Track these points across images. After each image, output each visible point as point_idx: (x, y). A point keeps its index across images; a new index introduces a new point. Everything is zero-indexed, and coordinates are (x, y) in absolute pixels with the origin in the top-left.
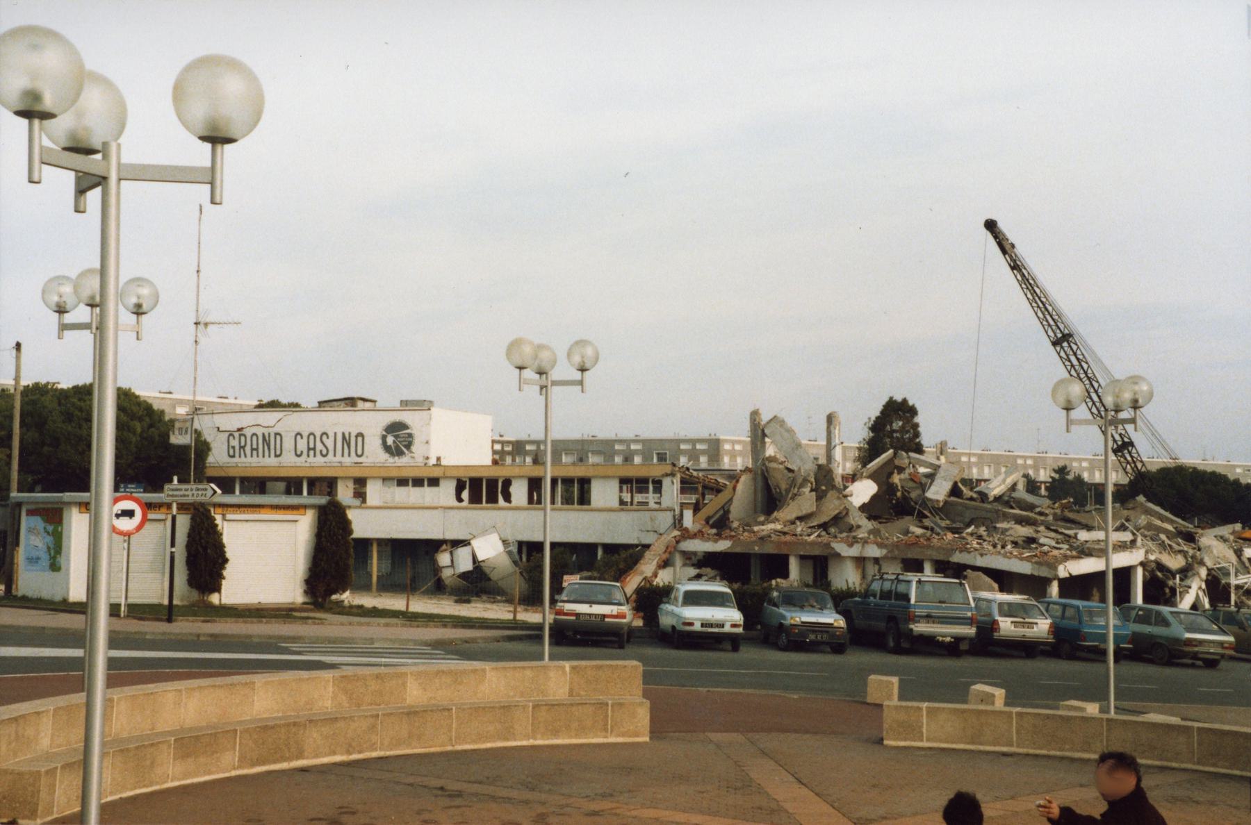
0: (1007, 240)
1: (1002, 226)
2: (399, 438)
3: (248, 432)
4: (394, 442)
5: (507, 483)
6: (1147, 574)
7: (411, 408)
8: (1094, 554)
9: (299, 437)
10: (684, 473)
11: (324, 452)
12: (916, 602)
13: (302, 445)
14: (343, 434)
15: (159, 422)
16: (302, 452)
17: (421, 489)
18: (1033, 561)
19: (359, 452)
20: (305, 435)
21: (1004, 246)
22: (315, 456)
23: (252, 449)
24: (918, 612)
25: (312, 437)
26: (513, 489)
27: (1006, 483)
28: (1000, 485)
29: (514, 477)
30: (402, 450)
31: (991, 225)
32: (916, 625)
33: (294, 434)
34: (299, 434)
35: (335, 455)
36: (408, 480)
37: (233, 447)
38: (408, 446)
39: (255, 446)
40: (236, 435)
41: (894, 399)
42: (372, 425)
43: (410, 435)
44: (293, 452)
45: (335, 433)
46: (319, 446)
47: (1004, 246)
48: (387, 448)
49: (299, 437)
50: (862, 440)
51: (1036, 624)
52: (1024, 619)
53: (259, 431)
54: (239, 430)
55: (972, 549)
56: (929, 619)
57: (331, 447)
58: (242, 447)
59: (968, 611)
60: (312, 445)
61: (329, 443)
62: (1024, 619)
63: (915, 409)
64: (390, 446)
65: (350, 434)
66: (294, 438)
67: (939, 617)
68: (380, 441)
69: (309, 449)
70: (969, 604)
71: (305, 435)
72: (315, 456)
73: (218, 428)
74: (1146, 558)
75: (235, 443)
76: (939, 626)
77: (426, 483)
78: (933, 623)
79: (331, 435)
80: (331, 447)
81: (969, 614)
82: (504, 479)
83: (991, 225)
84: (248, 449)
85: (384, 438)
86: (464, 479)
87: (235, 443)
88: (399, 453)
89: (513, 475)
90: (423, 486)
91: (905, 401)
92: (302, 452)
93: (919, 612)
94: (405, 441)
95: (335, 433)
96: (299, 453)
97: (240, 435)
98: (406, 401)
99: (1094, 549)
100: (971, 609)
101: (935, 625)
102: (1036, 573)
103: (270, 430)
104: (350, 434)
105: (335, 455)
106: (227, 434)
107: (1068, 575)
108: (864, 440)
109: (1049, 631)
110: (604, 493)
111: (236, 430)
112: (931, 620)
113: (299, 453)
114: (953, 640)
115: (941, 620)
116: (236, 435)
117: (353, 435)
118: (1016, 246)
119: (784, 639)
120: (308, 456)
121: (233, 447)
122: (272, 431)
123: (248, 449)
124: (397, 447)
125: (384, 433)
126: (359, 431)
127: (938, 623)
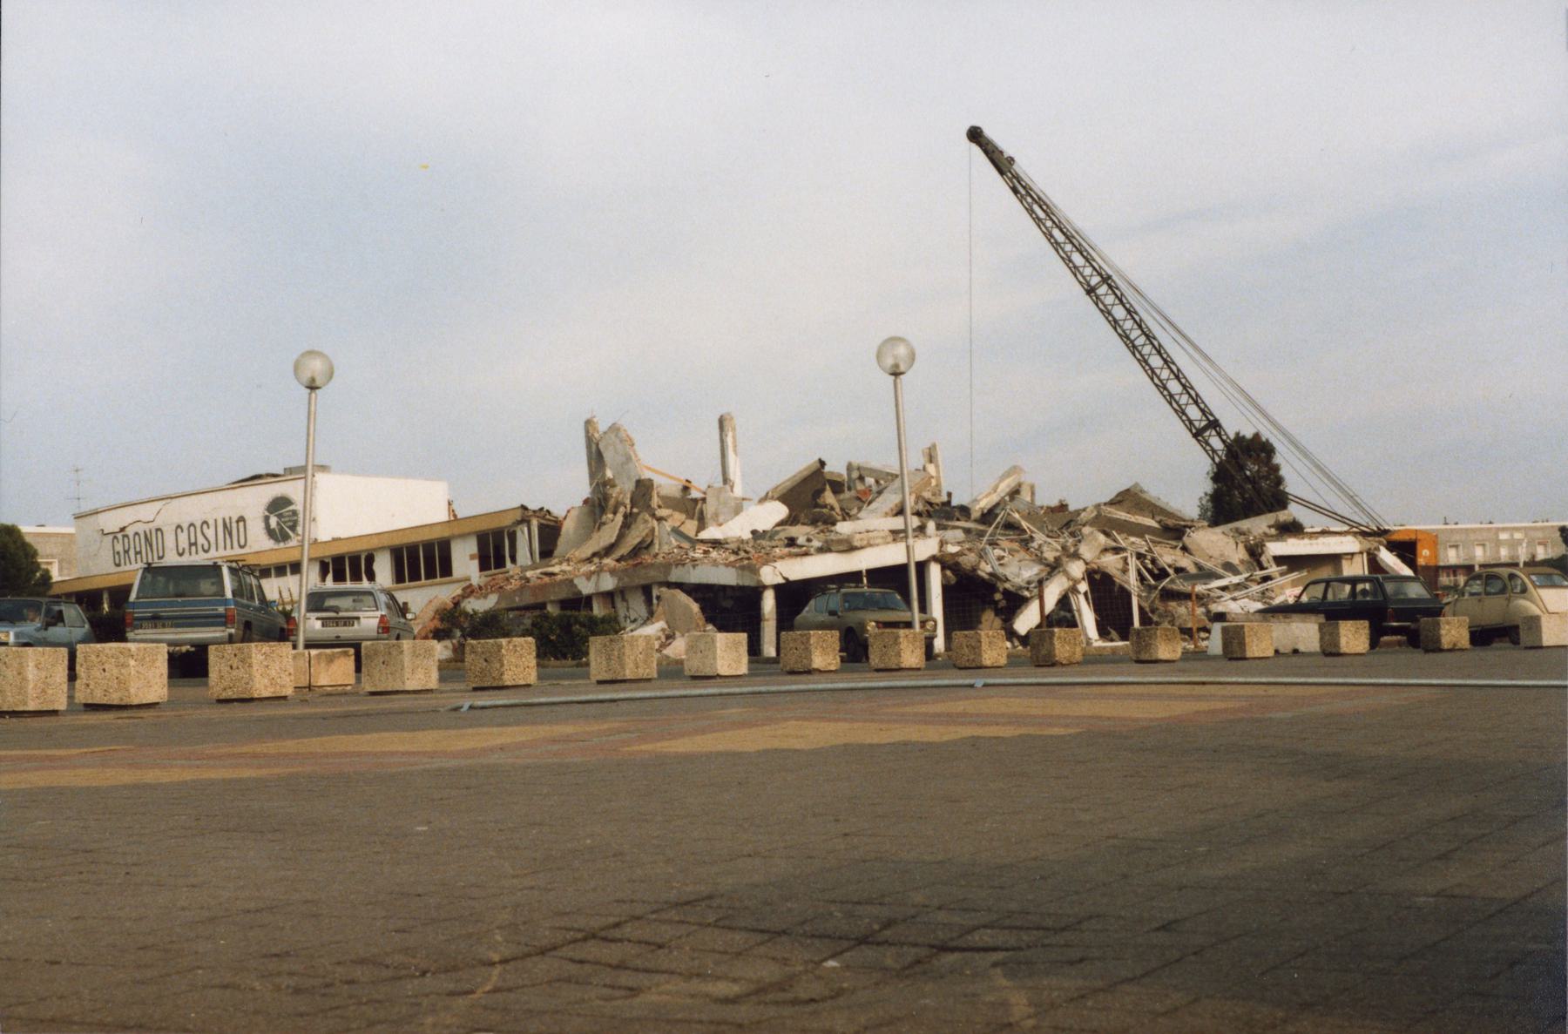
0: (1001, 152)
1: (990, 132)
2: (283, 517)
3: (130, 531)
4: (278, 524)
5: (370, 559)
6: (948, 573)
7: (297, 476)
8: (833, 548)
9: (179, 530)
10: (543, 518)
11: (206, 547)
12: (138, 598)
13: (183, 538)
14: (224, 520)
15: (528, 582)
16: (184, 549)
17: (269, 579)
18: (737, 565)
19: (242, 543)
20: (185, 526)
21: (1000, 162)
22: (197, 553)
23: (137, 553)
24: (136, 613)
25: (192, 528)
26: (376, 567)
27: (999, 490)
28: (989, 494)
29: (375, 550)
30: (287, 533)
31: (975, 135)
32: (136, 631)
33: (174, 528)
34: (179, 527)
35: (217, 550)
36: (270, 569)
37: (118, 553)
38: (293, 528)
39: (138, 549)
40: (120, 536)
41: (1241, 435)
42: (254, 501)
43: (295, 513)
44: (175, 552)
45: (216, 521)
46: (201, 540)
47: (1000, 162)
48: (271, 533)
49: (179, 530)
50: (1203, 495)
51: (358, 618)
52: (337, 613)
53: (140, 528)
54: (123, 529)
55: (688, 560)
56: (157, 621)
57: (212, 540)
58: (126, 552)
59: (221, 605)
60: (193, 540)
61: (210, 533)
62: (337, 613)
63: (1271, 445)
64: (274, 529)
65: (230, 518)
66: (174, 532)
67: (169, 618)
68: (262, 525)
69: (191, 545)
70: (223, 595)
71: (185, 526)
72: (197, 553)
73: (103, 530)
74: (940, 551)
75: (119, 548)
76: (173, 630)
77: (288, 570)
78: (164, 626)
79: (211, 522)
80: (212, 540)
81: (221, 609)
82: (366, 554)
83: (975, 135)
84: (132, 553)
85: (267, 519)
86: (327, 560)
87: (119, 548)
88: (286, 537)
89: (374, 547)
90: (270, 576)
91: (1257, 436)
92: (184, 549)
93: (139, 612)
94: (290, 521)
95: (216, 521)
96: (181, 551)
97: (124, 536)
98: (290, 469)
99: (832, 540)
100: (226, 602)
101: (167, 630)
102: (741, 584)
103: (151, 525)
104: (230, 518)
105: (217, 550)
106: (111, 537)
107: (783, 581)
108: (1206, 494)
109: (378, 627)
110: (465, 561)
111: (118, 530)
112: (160, 623)
113: (181, 551)
114: (193, 649)
115: (175, 621)
116: (120, 536)
117: (234, 520)
118: (1015, 159)
119: (72, 673)
120: (190, 554)
121: (118, 553)
122: (152, 526)
123: (132, 553)
124: (282, 529)
125: (267, 513)
126: (239, 515)
127: (172, 627)
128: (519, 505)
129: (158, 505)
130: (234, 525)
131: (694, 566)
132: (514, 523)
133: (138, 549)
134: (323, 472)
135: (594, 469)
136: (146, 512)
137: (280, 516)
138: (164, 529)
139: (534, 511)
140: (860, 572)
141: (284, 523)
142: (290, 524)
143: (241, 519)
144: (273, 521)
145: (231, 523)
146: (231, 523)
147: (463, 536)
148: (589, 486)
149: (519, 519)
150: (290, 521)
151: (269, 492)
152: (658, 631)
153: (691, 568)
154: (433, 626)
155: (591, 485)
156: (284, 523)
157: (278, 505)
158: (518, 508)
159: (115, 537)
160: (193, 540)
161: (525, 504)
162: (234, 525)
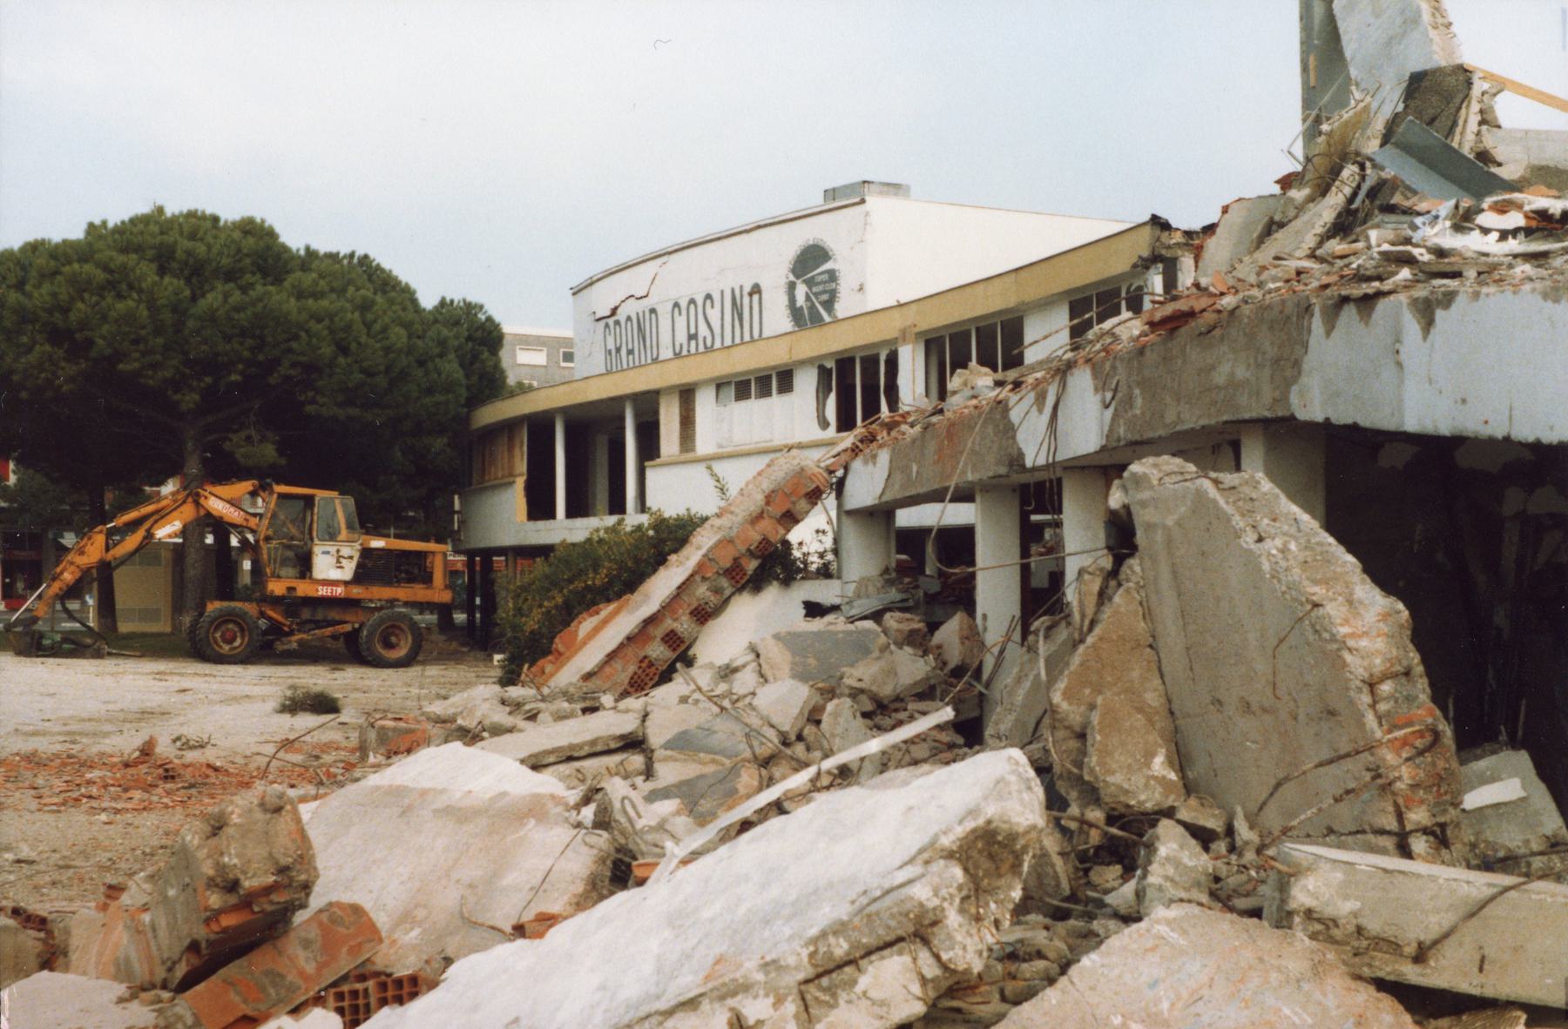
4: (808, 298)
36: (749, 381)
38: (829, 305)
45: (722, 292)
48: (796, 313)
57: (717, 330)
58: (618, 350)
65: (741, 287)
71: (684, 304)
84: (624, 351)
85: (791, 287)
94: (825, 292)
95: (722, 292)
104: (741, 287)
117: (747, 289)
124: (812, 308)
125: (792, 278)
128: (1146, 217)
129: (652, 267)
130: (746, 300)
131: (1426, 312)
132: (1135, 266)
133: (630, 347)
134: (896, 194)
135: (1312, 82)
136: (634, 281)
137: (810, 283)
138: (659, 311)
139: (1189, 234)
140: (1060, 512)
141: (816, 294)
142: (825, 297)
143: (756, 290)
144: (801, 291)
145: (742, 297)
146: (742, 297)
147: (1045, 304)
148: (1300, 122)
149: (1146, 253)
150: (825, 292)
151: (792, 241)
152: (930, 854)
153: (1411, 325)
154: (758, 538)
155: (1304, 120)
156: (816, 294)
157: (811, 259)
158: (1144, 224)
159: (607, 326)
160: (693, 331)
161: (1164, 214)
162: (746, 300)
